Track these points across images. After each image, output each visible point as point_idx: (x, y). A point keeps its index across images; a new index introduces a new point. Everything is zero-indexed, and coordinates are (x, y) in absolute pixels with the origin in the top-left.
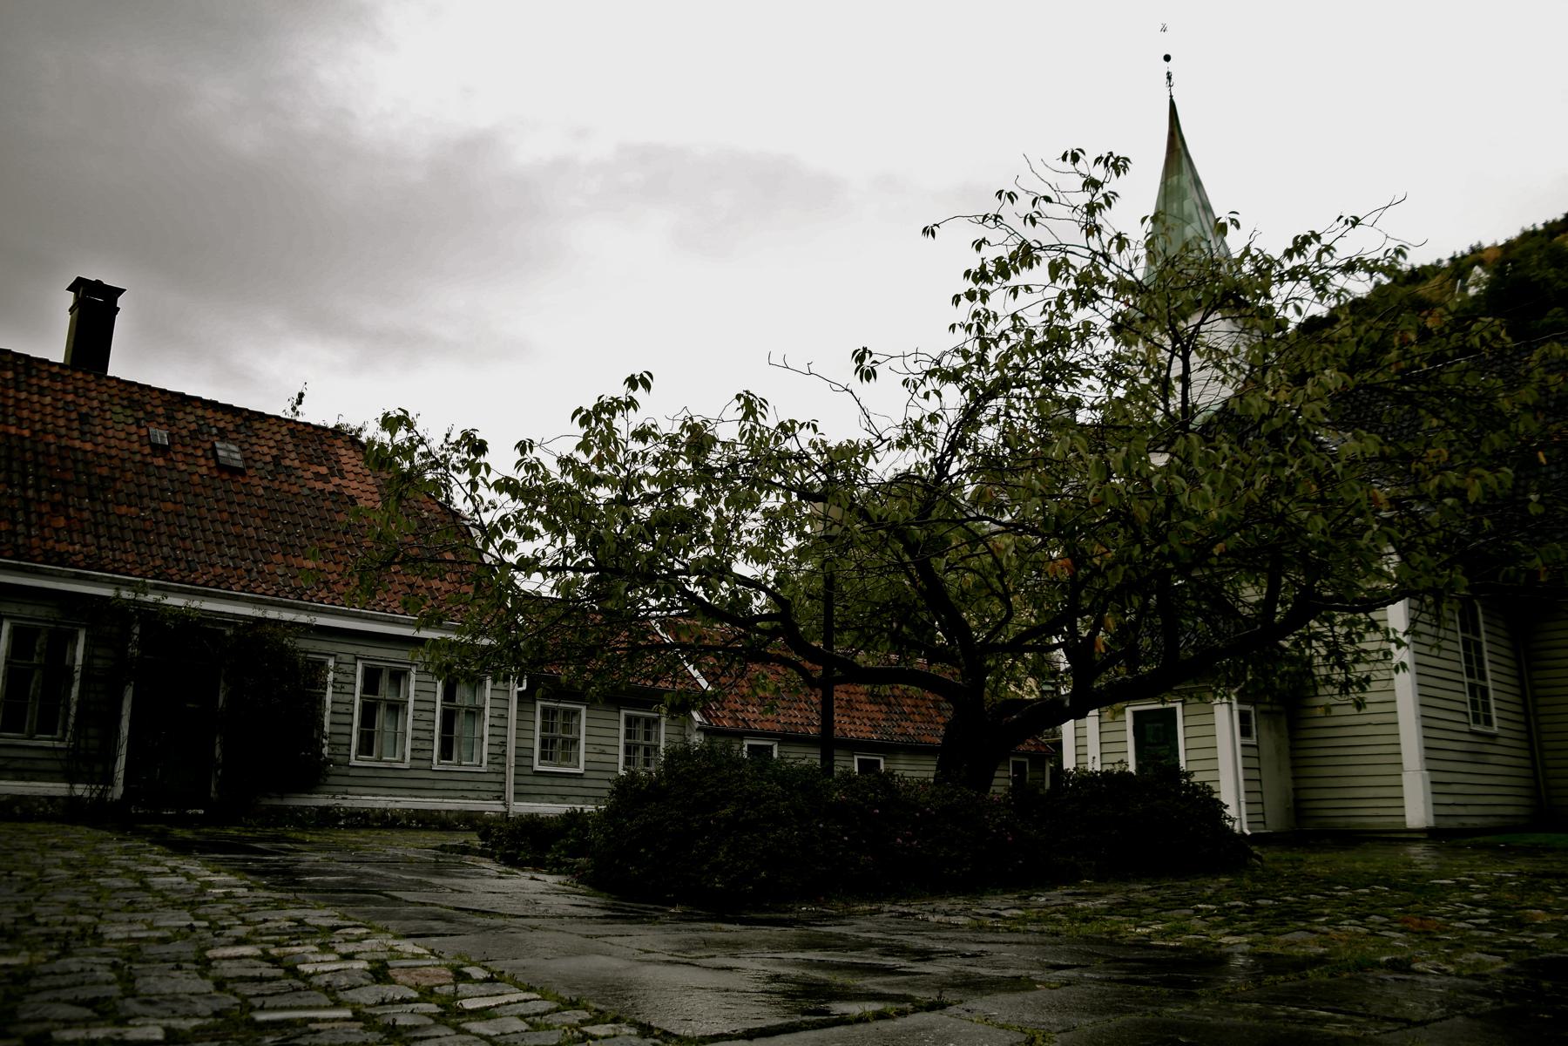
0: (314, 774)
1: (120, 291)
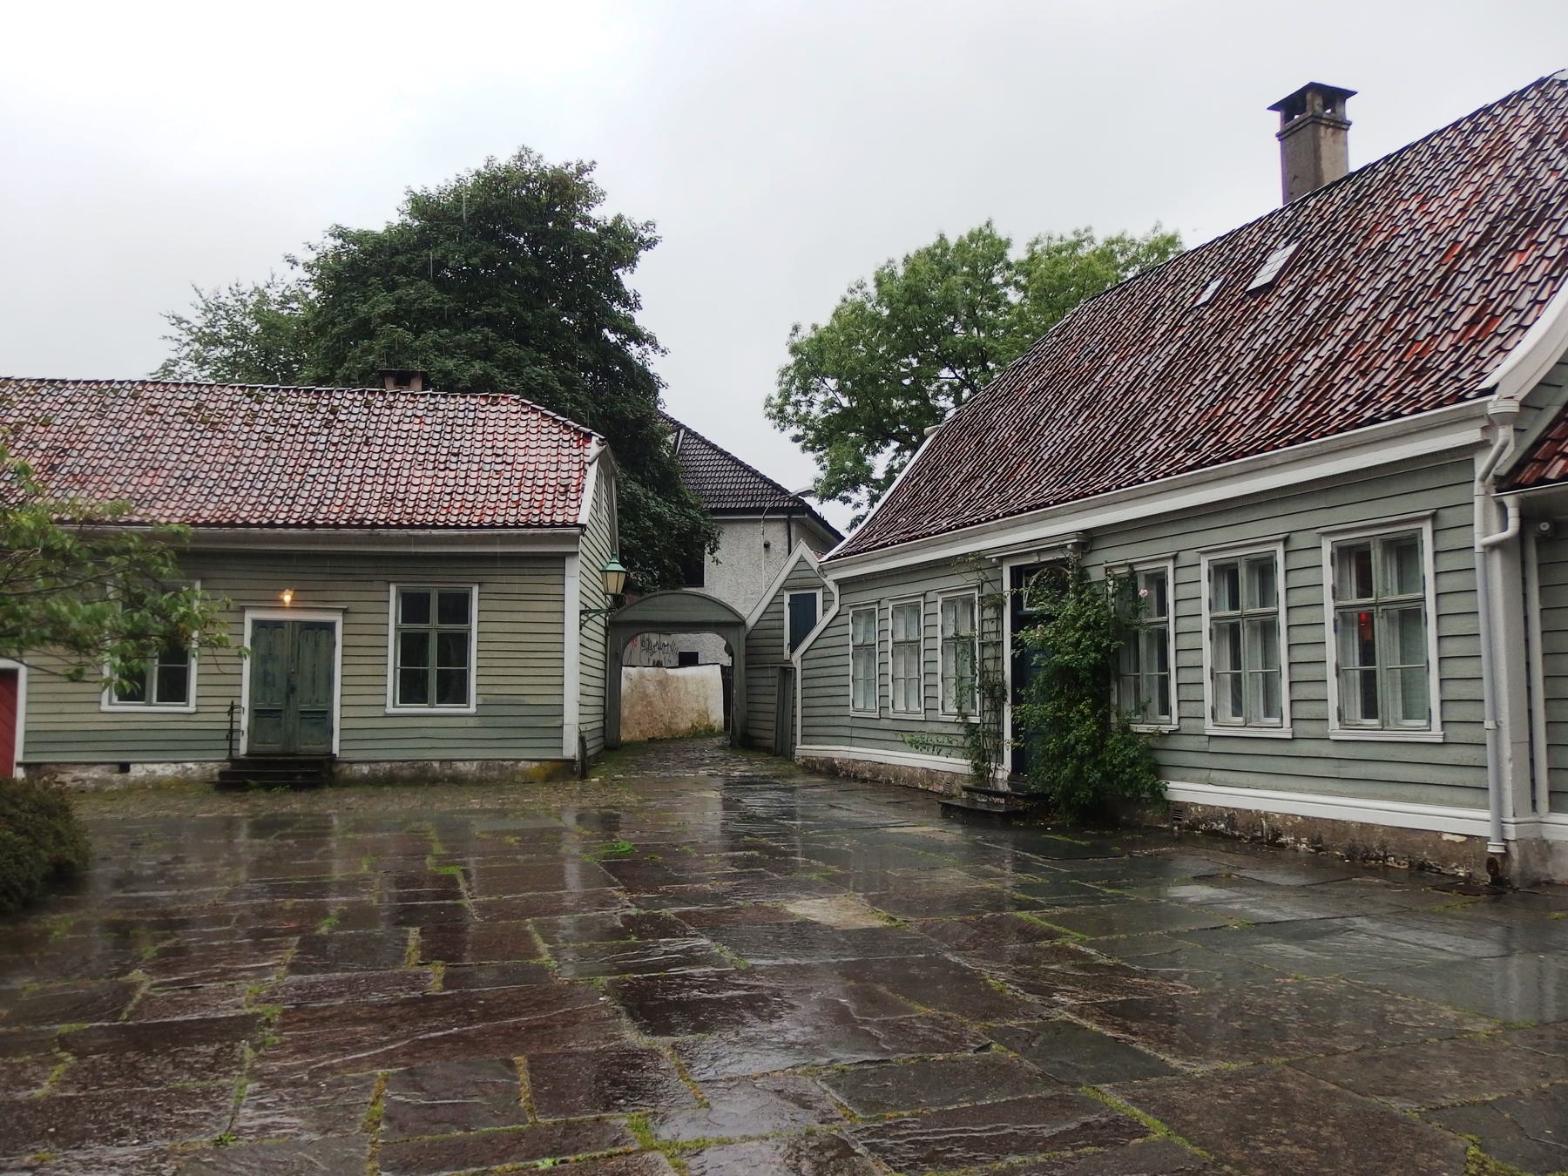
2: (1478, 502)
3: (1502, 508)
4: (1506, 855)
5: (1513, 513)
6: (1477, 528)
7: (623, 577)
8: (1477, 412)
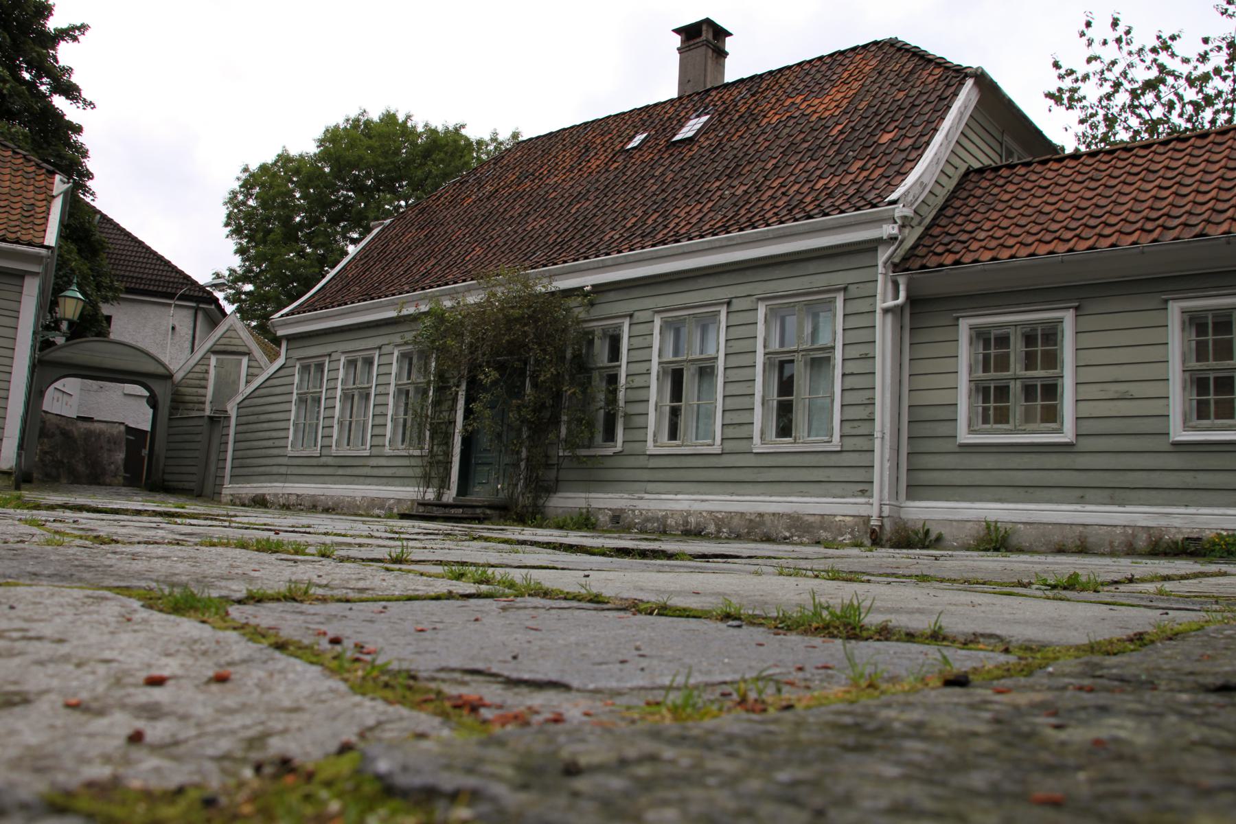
0: (594, 474)
1: (730, 34)
2: (880, 278)
3: (896, 285)
4: (881, 527)
5: (902, 289)
6: (879, 297)
7: (81, 305)
8: (886, 215)
